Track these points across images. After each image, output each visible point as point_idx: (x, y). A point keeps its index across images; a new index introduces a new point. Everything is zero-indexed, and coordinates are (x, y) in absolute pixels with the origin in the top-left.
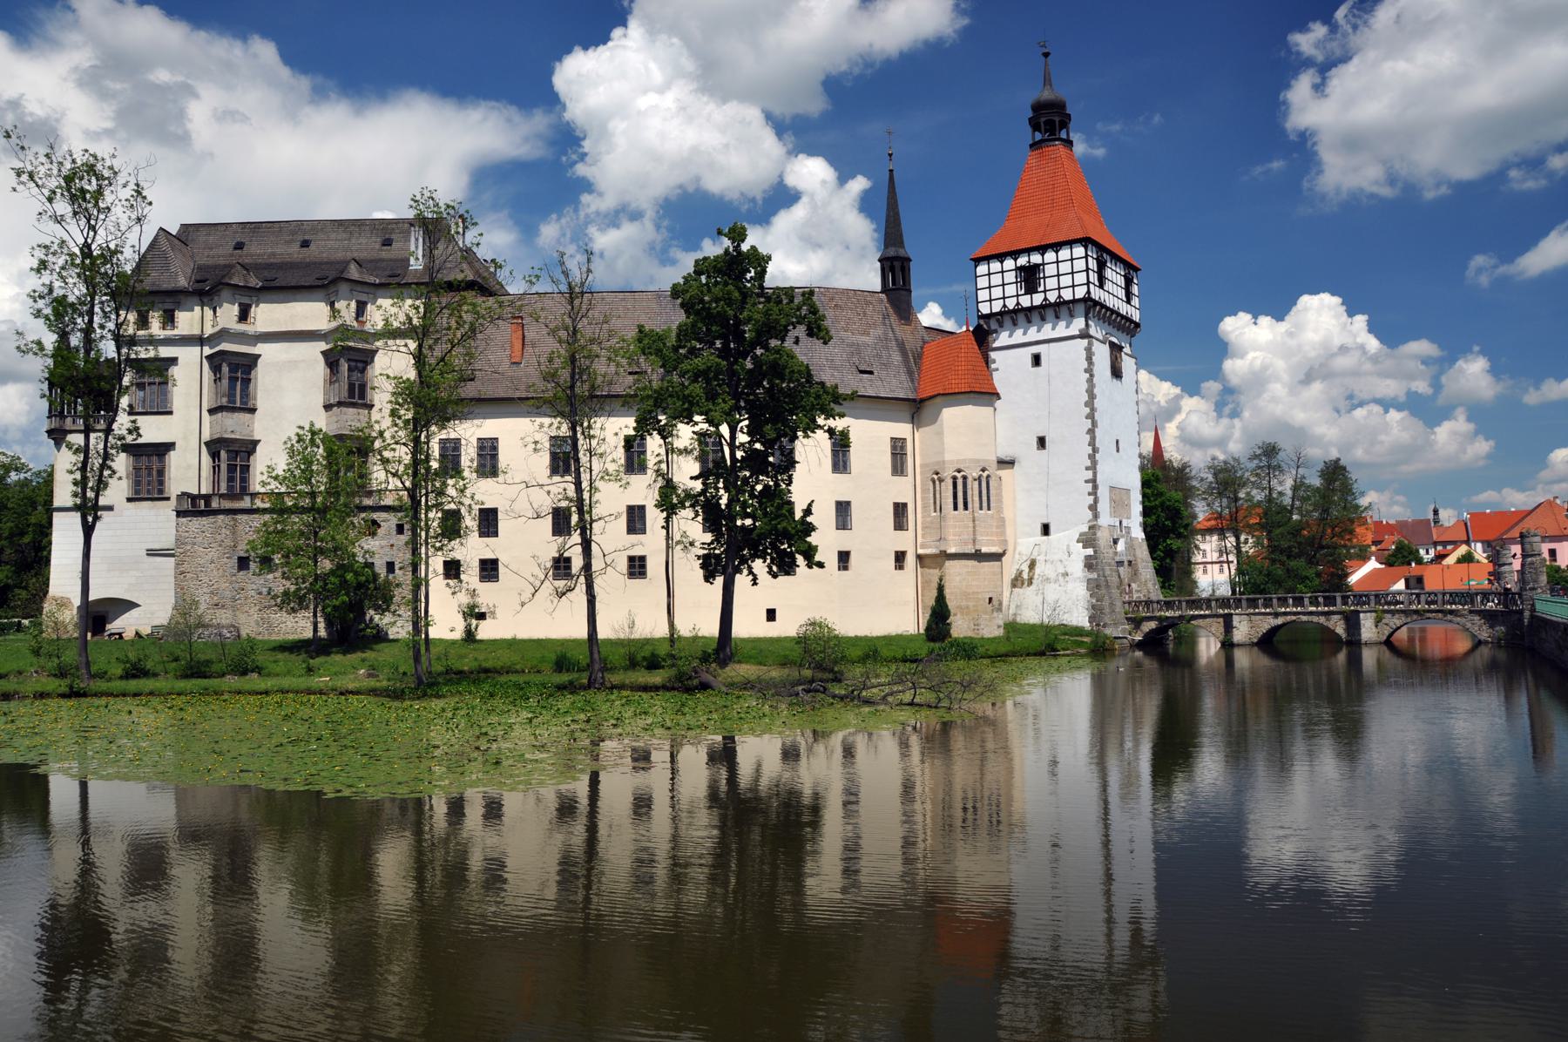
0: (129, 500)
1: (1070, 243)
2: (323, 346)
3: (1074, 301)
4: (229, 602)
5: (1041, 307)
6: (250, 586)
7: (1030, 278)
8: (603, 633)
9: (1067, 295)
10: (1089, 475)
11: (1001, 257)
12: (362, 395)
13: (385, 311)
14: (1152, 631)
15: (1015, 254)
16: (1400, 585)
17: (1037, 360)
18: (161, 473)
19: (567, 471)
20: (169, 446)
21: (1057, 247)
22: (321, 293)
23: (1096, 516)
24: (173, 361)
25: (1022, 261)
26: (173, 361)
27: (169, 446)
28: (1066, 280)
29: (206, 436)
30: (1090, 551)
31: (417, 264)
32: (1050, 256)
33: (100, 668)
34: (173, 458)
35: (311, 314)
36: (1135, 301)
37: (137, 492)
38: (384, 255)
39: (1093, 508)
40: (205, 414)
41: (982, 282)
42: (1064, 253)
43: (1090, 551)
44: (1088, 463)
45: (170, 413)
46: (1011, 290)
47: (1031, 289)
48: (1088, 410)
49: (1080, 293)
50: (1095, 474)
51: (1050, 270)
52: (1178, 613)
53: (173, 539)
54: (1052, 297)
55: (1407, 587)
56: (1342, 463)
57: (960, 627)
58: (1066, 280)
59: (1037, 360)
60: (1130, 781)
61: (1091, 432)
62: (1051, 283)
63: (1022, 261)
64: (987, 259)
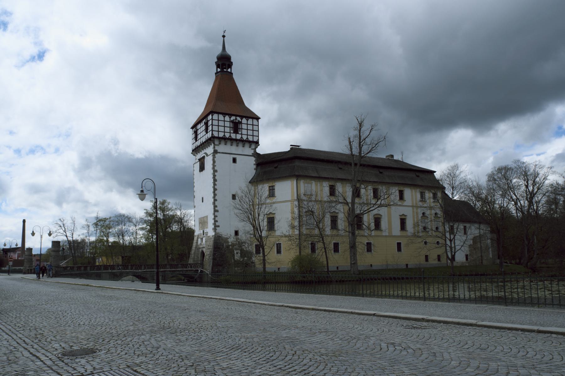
1: (218, 113)
3: (253, 142)
9: (250, 138)
15: (230, 115)
17: (234, 160)
25: (233, 118)
46: (227, 130)
54: (245, 137)
59: (234, 160)
62: (244, 132)
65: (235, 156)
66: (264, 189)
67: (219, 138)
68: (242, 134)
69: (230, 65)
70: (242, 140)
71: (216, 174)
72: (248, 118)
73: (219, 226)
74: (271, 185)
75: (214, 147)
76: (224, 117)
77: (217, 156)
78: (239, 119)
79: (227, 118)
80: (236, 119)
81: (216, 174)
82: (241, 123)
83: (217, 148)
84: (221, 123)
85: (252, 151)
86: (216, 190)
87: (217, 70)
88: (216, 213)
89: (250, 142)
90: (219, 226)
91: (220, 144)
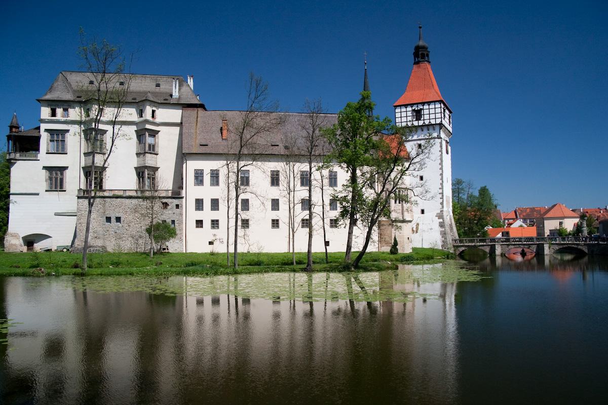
0: (46, 191)
2: (134, 128)
3: (436, 124)
4: (101, 236)
5: (422, 126)
6: (111, 230)
7: (418, 114)
8: (313, 250)
9: (433, 122)
10: (440, 191)
11: (406, 106)
12: (154, 150)
13: (164, 115)
14: (583, 251)
15: (412, 105)
16: (500, 235)
18: (62, 180)
19: (306, 185)
20: (66, 168)
21: (429, 103)
22: (135, 105)
23: (443, 207)
24: (68, 131)
25: (415, 107)
26: (68, 131)
27: (66, 168)
28: (432, 116)
29: (83, 165)
30: (441, 220)
31: (176, 94)
32: (426, 107)
33: (38, 265)
34: (67, 173)
35: (129, 113)
36: (451, 125)
37: (51, 187)
38: (90, 88)
39: (442, 204)
40: (82, 155)
41: (398, 115)
42: (432, 106)
43: (441, 220)
44: (440, 187)
45: (66, 154)
46: (409, 119)
47: (418, 119)
48: (440, 166)
49: (438, 121)
50: (443, 191)
51: (426, 112)
52: (473, 244)
53: (76, 209)
54: (427, 122)
55: (503, 236)
56: (487, 188)
57: (400, 250)
58: (432, 116)
60: (450, 305)
61: (442, 174)
62: (427, 117)
63: (415, 107)
64: (400, 106)
84: (432, 111)
86: (440, 169)
87: (415, 60)
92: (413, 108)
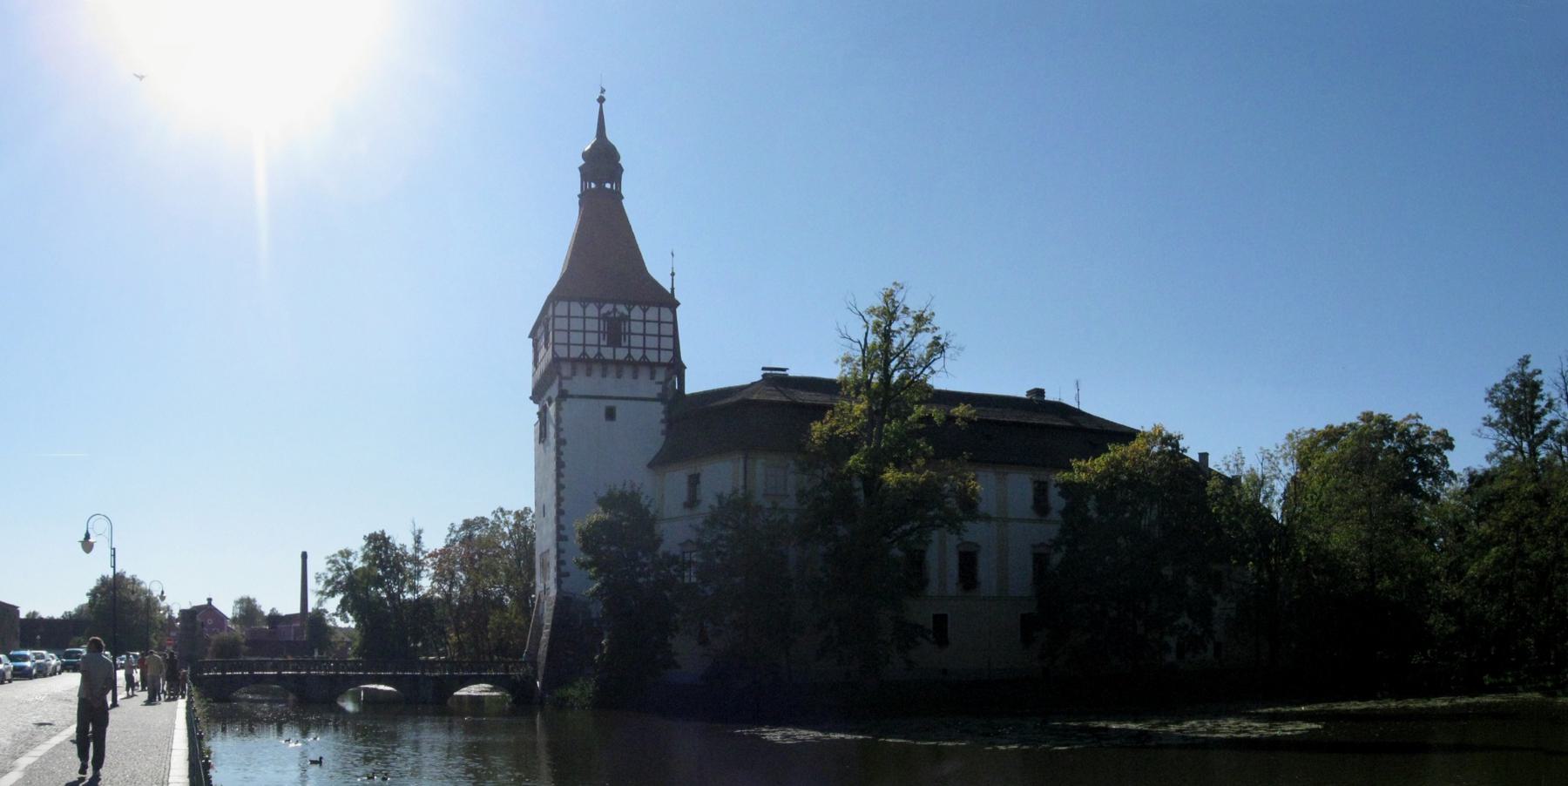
3: (659, 364)
9: (652, 356)
17: (610, 414)
25: (608, 308)
54: (637, 355)
59: (610, 414)
65: (611, 403)
66: (677, 479)
67: (568, 360)
68: (629, 347)
69: (615, 172)
70: (629, 362)
71: (562, 448)
72: (645, 304)
73: (567, 575)
74: (692, 472)
75: (560, 384)
76: (584, 308)
77: (564, 405)
78: (622, 309)
79: (592, 310)
80: (615, 310)
81: (562, 448)
82: (627, 319)
83: (566, 385)
85: (659, 389)
88: (562, 544)
89: (653, 367)
90: (567, 575)
91: (574, 374)
92: (604, 311)
